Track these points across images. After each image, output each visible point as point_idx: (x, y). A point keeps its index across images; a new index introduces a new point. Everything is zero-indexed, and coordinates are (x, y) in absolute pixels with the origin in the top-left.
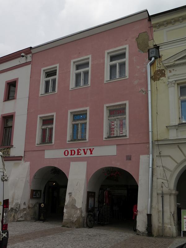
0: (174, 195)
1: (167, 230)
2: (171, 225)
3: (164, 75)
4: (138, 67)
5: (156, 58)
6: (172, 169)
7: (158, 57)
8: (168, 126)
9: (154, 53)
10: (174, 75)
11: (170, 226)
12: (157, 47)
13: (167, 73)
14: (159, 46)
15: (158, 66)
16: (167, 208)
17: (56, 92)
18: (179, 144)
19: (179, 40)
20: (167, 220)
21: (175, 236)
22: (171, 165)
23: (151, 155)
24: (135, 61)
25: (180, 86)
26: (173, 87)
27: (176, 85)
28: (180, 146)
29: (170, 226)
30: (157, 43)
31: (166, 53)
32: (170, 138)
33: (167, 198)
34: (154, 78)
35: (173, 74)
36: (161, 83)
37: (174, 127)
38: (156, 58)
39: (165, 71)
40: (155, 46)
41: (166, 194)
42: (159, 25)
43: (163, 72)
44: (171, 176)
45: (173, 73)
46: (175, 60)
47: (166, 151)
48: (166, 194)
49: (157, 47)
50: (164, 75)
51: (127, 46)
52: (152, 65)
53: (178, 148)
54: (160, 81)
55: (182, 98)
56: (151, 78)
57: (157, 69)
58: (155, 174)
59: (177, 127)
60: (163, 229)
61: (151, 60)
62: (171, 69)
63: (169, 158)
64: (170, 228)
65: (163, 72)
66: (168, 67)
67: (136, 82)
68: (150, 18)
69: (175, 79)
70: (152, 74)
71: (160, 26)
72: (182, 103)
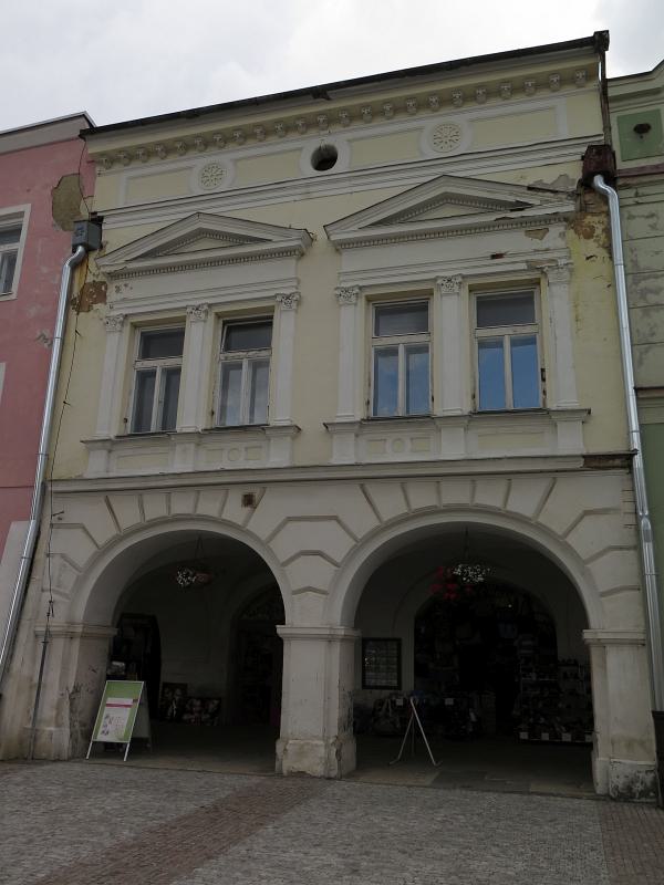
0: (344, 640)
1: (43, 739)
2: (58, 725)
3: (102, 297)
4: (45, 270)
5: (88, 250)
6: (338, 559)
7: (93, 246)
8: (330, 424)
9: (84, 234)
10: (124, 299)
11: (53, 729)
12: (97, 220)
13: (112, 295)
14: (101, 219)
15: (96, 268)
16: (53, 677)
17: (14, 297)
18: (107, 493)
19: (563, 144)
20: (47, 712)
21: (66, 753)
22: (82, 551)
23: (33, 523)
24: (40, 250)
25: (142, 334)
26: (456, 297)
27: (363, 300)
28: (371, 488)
29: (53, 729)
30: (98, 206)
31: (116, 234)
32: (86, 476)
33: (58, 645)
34: (77, 304)
35: (122, 296)
36: (89, 323)
37: (100, 444)
38: (88, 250)
39: (106, 288)
40: (94, 217)
41: (58, 635)
42: (111, 160)
43: (103, 288)
44: (80, 582)
45: (126, 293)
46: (362, 225)
47: (77, 511)
48: (58, 635)
49: (97, 220)
50: (102, 297)
51: (26, 208)
52: (75, 266)
53: (360, 492)
54: (91, 312)
55: (139, 365)
56: (69, 302)
57: (90, 279)
58: (36, 575)
59: (357, 427)
60: (34, 735)
61: (74, 252)
62: (121, 283)
63: (334, 522)
64: (51, 734)
65: (103, 288)
66: (113, 276)
67: (33, 311)
68: (91, 132)
69: (125, 312)
70: (76, 292)
71: (149, 156)
72: (412, 357)
